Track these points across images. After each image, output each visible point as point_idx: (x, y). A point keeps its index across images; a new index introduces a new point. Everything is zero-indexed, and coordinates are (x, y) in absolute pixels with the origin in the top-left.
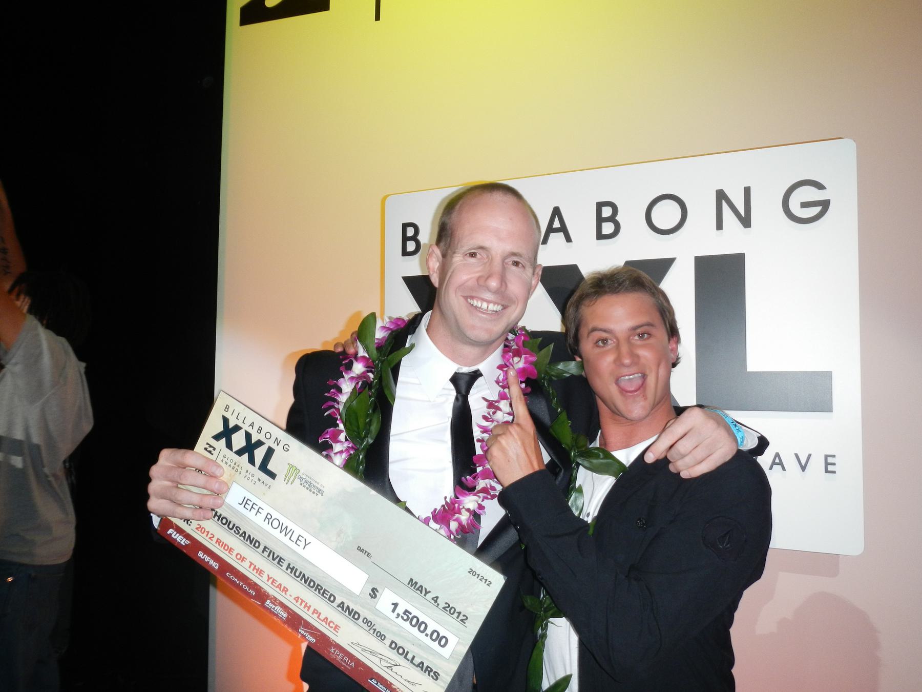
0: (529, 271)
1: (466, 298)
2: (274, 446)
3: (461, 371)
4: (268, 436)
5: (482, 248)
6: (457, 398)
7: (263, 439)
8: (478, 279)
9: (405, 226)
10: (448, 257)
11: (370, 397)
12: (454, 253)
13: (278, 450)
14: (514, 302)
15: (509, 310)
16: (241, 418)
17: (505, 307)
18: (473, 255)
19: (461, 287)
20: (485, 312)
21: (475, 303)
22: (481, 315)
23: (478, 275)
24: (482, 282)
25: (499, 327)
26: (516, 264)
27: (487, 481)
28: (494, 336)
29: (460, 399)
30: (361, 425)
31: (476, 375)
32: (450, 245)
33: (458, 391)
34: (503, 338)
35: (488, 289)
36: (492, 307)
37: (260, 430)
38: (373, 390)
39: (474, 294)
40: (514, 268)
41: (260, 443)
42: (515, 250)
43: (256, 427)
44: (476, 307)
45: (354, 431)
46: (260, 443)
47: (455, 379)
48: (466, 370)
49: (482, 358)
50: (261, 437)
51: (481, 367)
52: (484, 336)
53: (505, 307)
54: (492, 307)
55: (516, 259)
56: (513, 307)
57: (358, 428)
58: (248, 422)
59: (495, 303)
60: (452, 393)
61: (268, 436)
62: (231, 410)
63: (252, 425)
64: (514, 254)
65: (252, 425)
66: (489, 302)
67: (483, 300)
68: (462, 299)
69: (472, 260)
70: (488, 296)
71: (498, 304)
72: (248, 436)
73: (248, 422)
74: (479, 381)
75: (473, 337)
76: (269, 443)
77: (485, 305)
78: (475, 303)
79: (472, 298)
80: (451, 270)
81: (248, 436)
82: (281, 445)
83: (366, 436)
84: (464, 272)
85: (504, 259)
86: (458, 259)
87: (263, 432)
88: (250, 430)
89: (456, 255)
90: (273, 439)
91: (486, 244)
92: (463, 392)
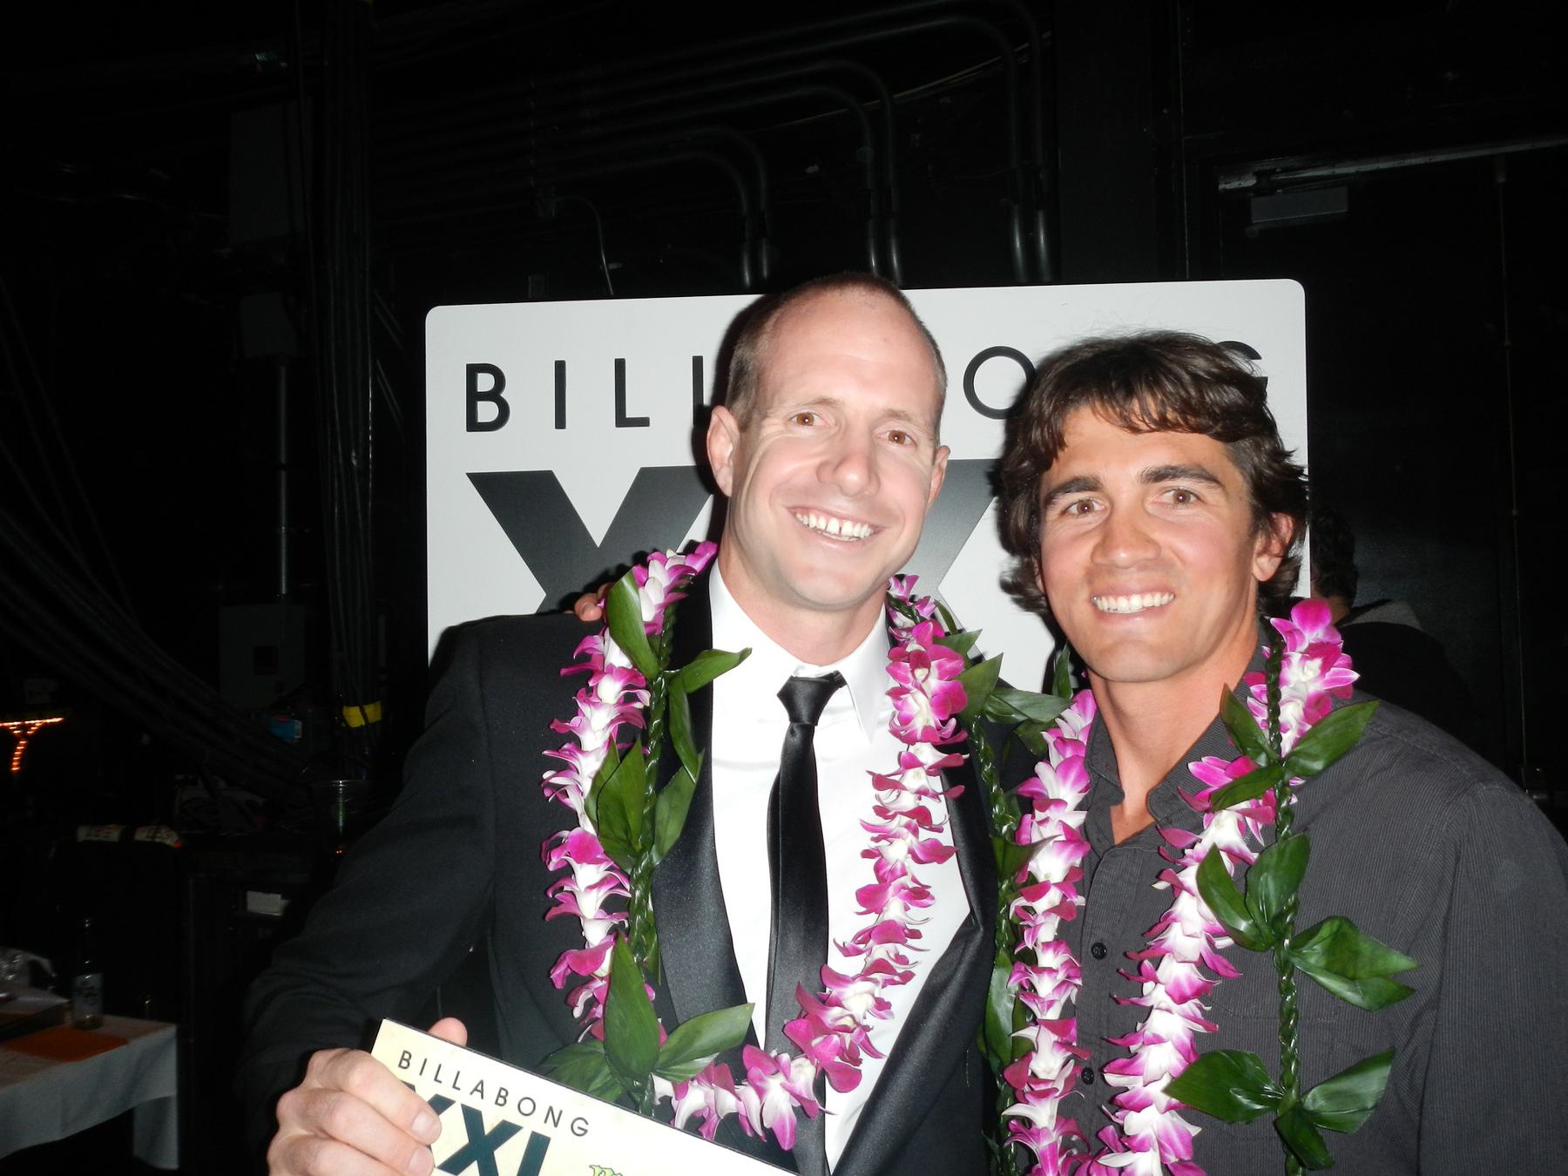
0: (926, 451)
1: (793, 510)
2: (546, 1130)
3: (802, 674)
4: (527, 1106)
5: (824, 402)
6: (791, 732)
7: (515, 1118)
8: (819, 469)
9: (473, 371)
10: (753, 427)
11: (647, 758)
12: (765, 417)
13: (560, 1139)
14: (896, 519)
15: (884, 538)
16: (447, 1076)
17: (876, 530)
18: (805, 419)
19: (782, 489)
20: (838, 539)
21: (813, 521)
22: (825, 543)
23: (817, 461)
24: (826, 475)
25: (865, 572)
26: (898, 437)
27: (890, 946)
28: (856, 592)
29: (798, 734)
30: (633, 820)
31: (833, 683)
32: (755, 405)
33: (794, 717)
34: (880, 595)
35: (842, 490)
36: (849, 529)
37: (502, 1097)
38: (653, 743)
39: (810, 503)
40: (894, 447)
41: (506, 1131)
42: (897, 407)
43: (491, 1093)
44: (816, 529)
45: (618, 840)
46: (506, 1131)
47: (787, 696)
48: (814, 671)
49: (845, 641)
50: (510, 1114)
51: (847, 667)
52: (829, 589)
53: (876, 530)
54: (849, 529)
55: (898, 426)
56: (895, 529)
57: (627, 830)
58: (467, 1083)
59: (855, 521)
60: (780, 720)
61: (527, 1106)
62: (416, 1063)
63: (479, 1089)
64: (894, 415)
65: (479, 1089)
66: (842, 518)
67: (830, 514)
68: (784, 513)
69: (805, 431)
70: (841, 504)
71: (863, 523)
72: (473, 1118)
73: (467, 1083)
74: (838, 699)
75: (810, 595)
76: (532, 1125)
77: (834, 526)
78: (813, 521)
79: (806, 510)
80: (760, 453)
81: (473, 1118)
82: (565, 1122)
83: (646, 848)
84: (787, 455)
85: (872, 428)
86: (772, 428)
87: (512, 1100)
88: (475, 1102)
89: (767, 422)
90: (541, 1111)
91: (835, 394)
92: (805, 720)
